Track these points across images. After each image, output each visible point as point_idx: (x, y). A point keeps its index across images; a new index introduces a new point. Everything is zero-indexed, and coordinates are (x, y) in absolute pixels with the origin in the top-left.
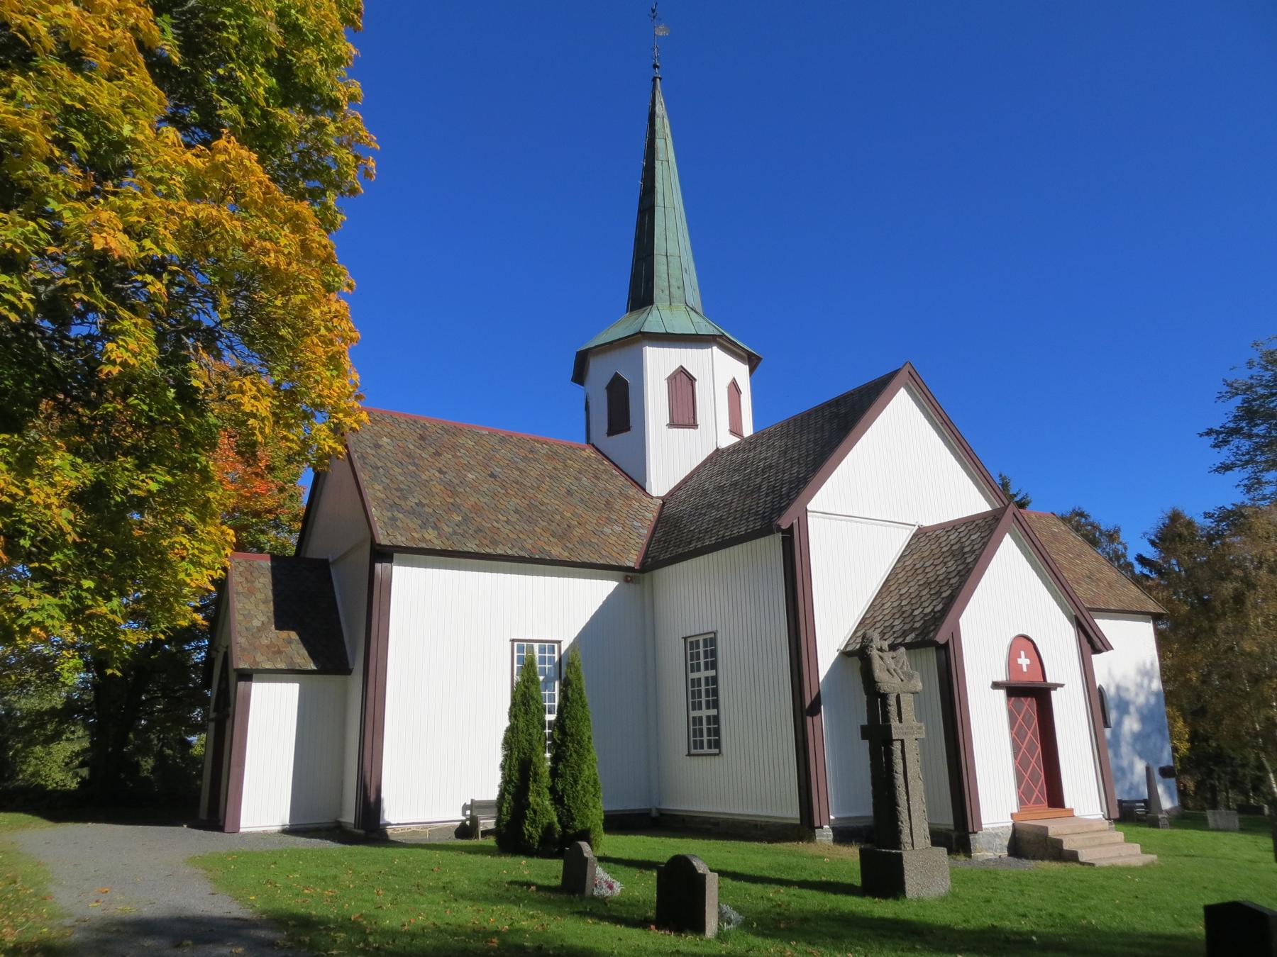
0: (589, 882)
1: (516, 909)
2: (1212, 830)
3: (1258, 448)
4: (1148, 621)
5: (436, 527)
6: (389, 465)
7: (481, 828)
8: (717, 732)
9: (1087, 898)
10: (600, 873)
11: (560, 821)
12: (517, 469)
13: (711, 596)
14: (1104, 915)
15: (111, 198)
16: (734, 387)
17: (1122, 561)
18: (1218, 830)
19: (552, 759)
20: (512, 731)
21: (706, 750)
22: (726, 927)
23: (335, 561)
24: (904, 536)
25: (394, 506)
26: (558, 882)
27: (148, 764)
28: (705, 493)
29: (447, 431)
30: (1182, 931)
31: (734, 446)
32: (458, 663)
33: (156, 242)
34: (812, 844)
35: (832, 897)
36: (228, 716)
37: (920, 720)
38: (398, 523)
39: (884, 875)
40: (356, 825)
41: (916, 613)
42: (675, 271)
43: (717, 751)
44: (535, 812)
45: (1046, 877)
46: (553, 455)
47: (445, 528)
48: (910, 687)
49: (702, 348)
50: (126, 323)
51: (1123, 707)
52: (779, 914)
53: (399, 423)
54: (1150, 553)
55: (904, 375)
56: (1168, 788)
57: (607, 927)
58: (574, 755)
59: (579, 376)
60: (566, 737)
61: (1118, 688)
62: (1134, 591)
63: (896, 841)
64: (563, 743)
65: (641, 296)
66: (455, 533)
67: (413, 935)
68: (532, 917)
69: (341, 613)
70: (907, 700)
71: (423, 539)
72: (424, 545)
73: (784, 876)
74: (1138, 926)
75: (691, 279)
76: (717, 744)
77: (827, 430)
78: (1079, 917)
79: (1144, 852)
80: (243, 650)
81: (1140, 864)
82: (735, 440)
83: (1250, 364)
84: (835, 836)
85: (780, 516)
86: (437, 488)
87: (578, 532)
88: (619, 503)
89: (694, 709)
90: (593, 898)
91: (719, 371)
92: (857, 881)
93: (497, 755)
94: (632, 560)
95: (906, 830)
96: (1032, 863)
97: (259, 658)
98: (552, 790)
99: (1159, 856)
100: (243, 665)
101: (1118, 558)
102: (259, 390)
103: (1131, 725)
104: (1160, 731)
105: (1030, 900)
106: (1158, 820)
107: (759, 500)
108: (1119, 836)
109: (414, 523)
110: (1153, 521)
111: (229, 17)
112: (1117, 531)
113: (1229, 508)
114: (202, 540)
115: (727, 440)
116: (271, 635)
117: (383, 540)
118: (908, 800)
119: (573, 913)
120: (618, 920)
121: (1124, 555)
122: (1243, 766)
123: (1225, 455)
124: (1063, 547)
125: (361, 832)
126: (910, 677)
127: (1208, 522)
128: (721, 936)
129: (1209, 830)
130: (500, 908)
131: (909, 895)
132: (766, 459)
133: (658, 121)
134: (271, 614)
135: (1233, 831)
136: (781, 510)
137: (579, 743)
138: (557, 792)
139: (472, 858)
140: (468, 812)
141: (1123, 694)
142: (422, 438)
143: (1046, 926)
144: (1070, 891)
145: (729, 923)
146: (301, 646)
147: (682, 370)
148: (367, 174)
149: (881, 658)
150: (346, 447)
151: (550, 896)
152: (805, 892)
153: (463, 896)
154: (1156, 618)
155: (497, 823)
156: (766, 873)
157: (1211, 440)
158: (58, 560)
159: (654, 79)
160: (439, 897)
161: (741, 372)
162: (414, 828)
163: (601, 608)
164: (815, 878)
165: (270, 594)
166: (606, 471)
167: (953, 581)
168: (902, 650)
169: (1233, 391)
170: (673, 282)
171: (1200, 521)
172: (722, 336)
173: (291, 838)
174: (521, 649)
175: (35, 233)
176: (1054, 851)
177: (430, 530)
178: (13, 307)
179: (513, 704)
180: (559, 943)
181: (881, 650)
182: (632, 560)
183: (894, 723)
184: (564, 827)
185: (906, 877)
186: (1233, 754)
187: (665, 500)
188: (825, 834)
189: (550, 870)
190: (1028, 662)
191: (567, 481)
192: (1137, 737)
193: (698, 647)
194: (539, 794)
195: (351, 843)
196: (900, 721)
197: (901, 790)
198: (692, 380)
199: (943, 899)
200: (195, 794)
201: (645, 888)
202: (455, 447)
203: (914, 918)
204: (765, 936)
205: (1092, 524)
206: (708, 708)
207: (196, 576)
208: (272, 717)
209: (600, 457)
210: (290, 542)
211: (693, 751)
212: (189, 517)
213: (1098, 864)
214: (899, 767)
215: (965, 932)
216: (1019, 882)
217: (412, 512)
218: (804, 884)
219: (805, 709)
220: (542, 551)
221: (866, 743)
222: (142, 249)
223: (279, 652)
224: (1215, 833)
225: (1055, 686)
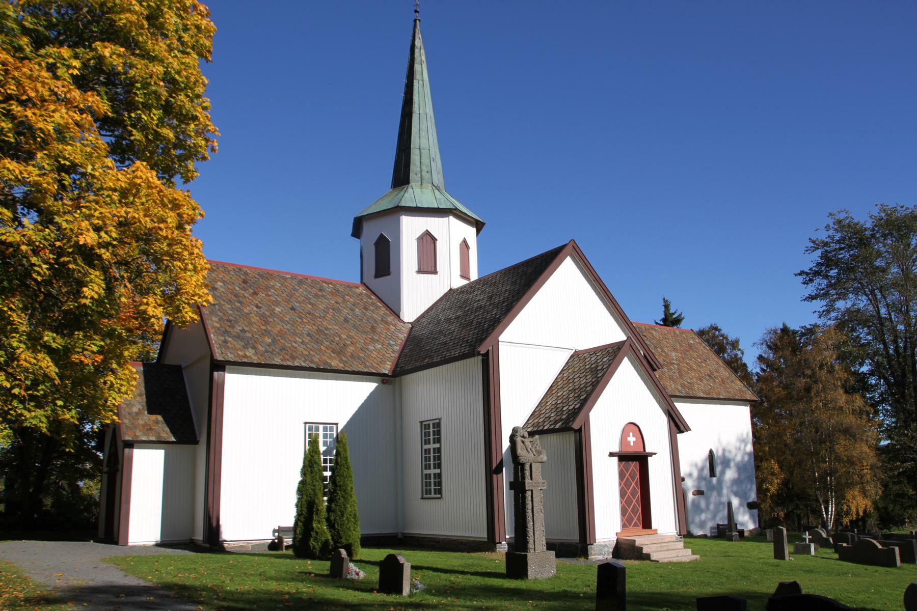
3: (830, 285)
5: (254, 348)
6: (222, 303)
7: (285, 544)
8: (440, 484)
12: (310, 304)
13: (436, 394)
15: (84, 210)
16: (465, 245)
19: (328, 501)
20: (302, 483)
21: (433, 495)
23: (186, 367)
25: (226, 332)
26: (328, 572)
27: (48, 501)
28: (439, 322)
29: (262, 276)
31: (465, 286)
32: (271, 433)
33: (106, 233)
36: (117, 470)
38: (229, 345)
39: (517, 565)
40: (204, 541)
42: (425, 160)
44: (317, 533)
46: (336, 293)
47: (260, 347)
48: (539, 459)
50: (92, 276)
51: (726, 463)
53: (229, 271)
55: (569, 249)
57: (350, 592)
58: (342, 499)
59: (357, 232)
60: (337, 489)
61: (724, 450)
62: (739, 385)
64: (335, 491)
65: (401, 178)
66: (266, 351)
67: (243, 594)
69: (190, 398)
71: (246, 356)
72: (246, 360)
75: (437, 166)
76: (439, 491)
77: (522, 280)
80: (127, 427)
82: (465, 282)
83: (827, 228)
85: (480, 345)
86: (255, 319)
87: (351, 349)
88: (380, 328)
91: (452, 233)
92: (503, 569)
93: (294, 498)
94: (387, 369)
95: (531, 541)
97: (138, 433)
98: (328, 520)
100: (128, 438)
102: (156, 302)
103: (730, 474)
104: (749, 478)
107: (471, 328)
109: (239, 344)
111: (138, 89)
113: (809, 327)
114: (121, 379)
116: (145, 418)
117: (219, 357)
124: (695, 355)
125: (207, 545)
126: (539, 453)
128: (411, 595)
130: (292, 584)
131: (530, 577)
133: (417, 51)
134: (144, 404)
136: (481, 340)
139: (277, 560)
140: (277, 534)
141: (727, 454)
142: (245, 282)
146: (165, 425)
147: (427, 233)
148: (213, 149)
149: (523, 442)
150: (201, 316)
151: (320, 578)
153: (271, 578)
155: (294, 539)
156: (456, 569)
158: (43, 389)
159: (415, 21)
160: (257, 579)
161: (470, 233)
162: (241, 543)
163: (366, 401)
165: (143, 389)
169: (816, 245)
170: (424, 168)
173: (163, 549)
174: (310, 429)
175: (49, 235)
177: (250, 349)
178: (39, 273)
179: (304, 467)
181: (523, 437)
183: (528, 480)
187: (413, 324)
189: (324, 566)
190: (634, 439)
192: (736, 482)
194: (319, 522)
195: (201, 552)
197: (530, 519)
198: (434, 240)
200: (104, 521)
201: (375, 575)
202: (267, 288)
205: (722, 335)
207: (118, 399)
208: (147, 470)
209: (369, 293)
210: (154, 350)
211: (425, 496)
212: (115, 366)
214: (529, 506)
217: (237, 337)
219: (492, 471)
220: (326, 363)
222: (100, 237)
223: (151, 429)
225: (651, 454)
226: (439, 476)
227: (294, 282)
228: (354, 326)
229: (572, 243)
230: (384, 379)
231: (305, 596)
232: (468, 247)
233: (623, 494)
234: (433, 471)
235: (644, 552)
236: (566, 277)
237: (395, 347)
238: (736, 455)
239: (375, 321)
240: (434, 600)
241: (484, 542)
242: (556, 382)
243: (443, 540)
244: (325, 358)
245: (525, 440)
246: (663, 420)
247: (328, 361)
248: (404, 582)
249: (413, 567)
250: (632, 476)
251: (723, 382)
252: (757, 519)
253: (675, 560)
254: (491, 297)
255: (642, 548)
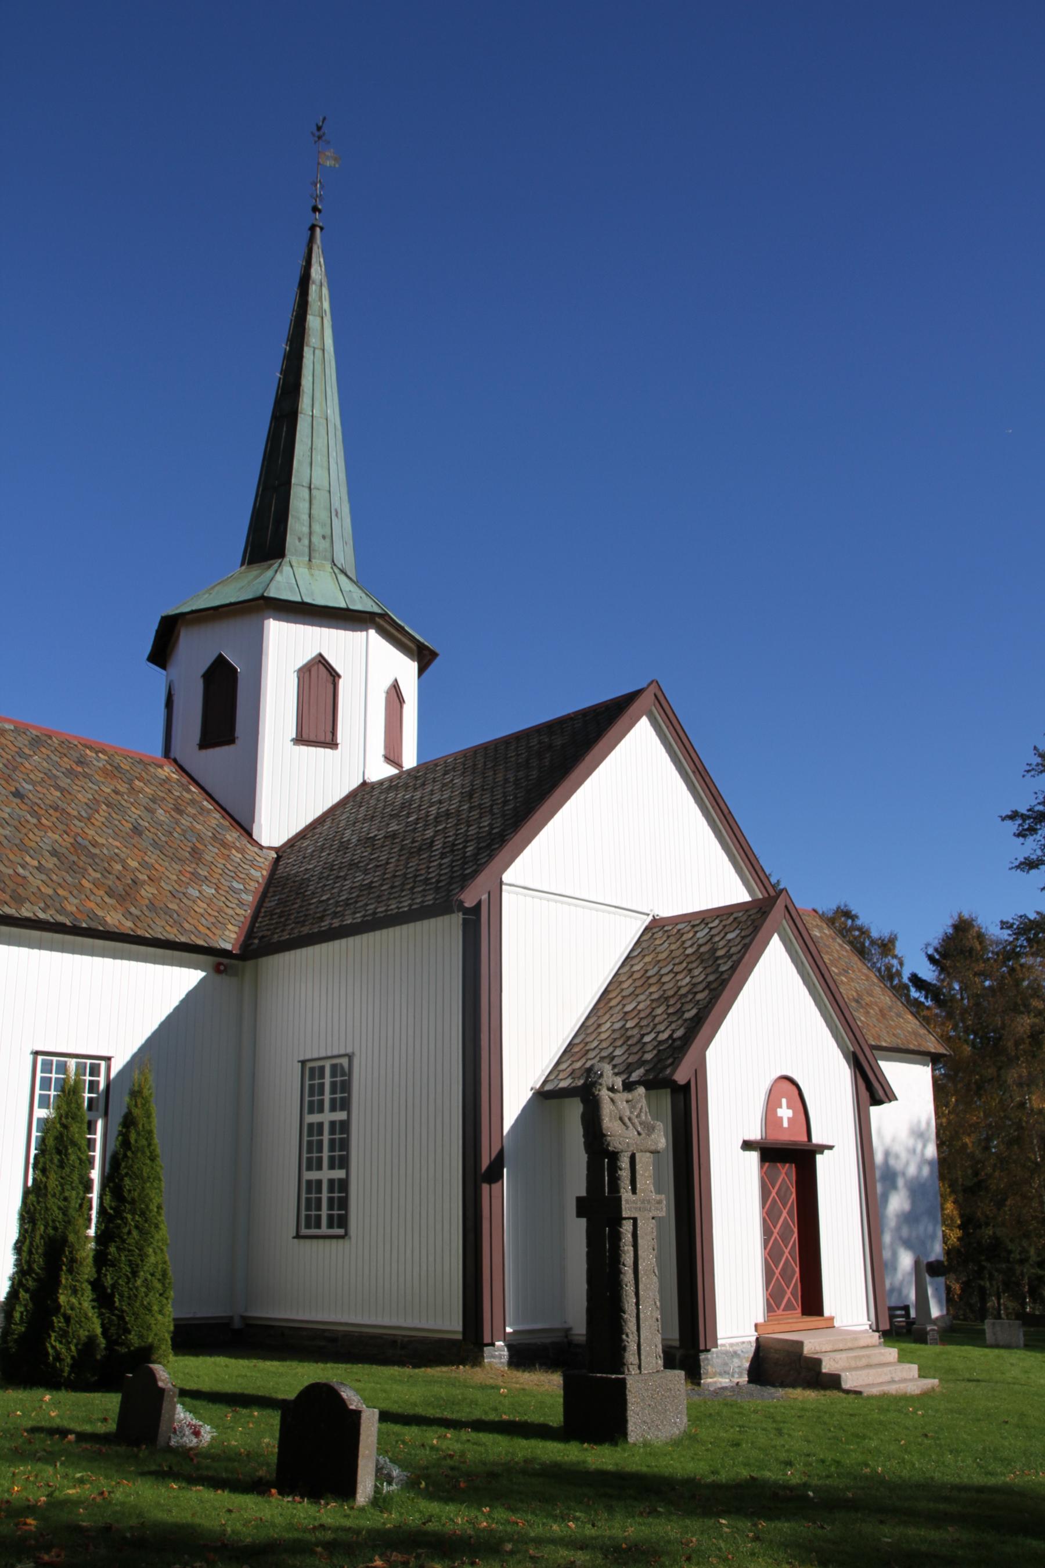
0: (163, 1427)
1: (50, 1469)
2: (991, 1346)
4: (925, 1064)
9: (864, 1437)
10: (182, 1414)
11: (105, 1333)
12: (58, 787)
13: (334, 1002)
14: (893, 1460)
16: (395, 693)
17: (896, 982)
18: (997, 1346)
21: (324, 1230)
22: (386, 1488)
24: (635, 928)
28: (344, 847)
30: (992, 1481)
31: (391, 779)
34: (478, 1369)
35: (524, 1442)
37: (658, 1191)
39: (597, 1407)
41: (647, 1039)
42: (321, 513)
43: (341, 1232)
44: (67, 1319)
45: (803, 1409)
46: (113, 771)
48: (650, 1144)
49: (353, 630)
52: (452, 1468)
54: (928, 973)
55: (646, 700)
56: (936, 1290)
58: (135, 1233)
59: (161, 654)
61: (887, 1154)
62: (911, 1023)
63: (617, 1363)
64: (118, 1213)
65: (267, 542)
68: (81, 1481)
70: (645, 1163)
73: (447, 1414)
74: (937, 1475)
75: (343, 527)
76: (342, 1222)
77: (534, 769)
78: (859, 1464)
79: (921, 1376)
81: (918, 1392)
82: (392, 771)
84: (511, 1356)
85: (463, 888)
87: (148, 891)
88: (211, 852)
89: (309, 1168)
90: (169, 1449)
91: (373, 668)
92: (555, 1417)
94: (229, 939)
95: (632, 1347)
96: (781, 1392)
98: (96, 1285)
99: (941, 1380)
101: (891, 977)
105: (789, 1442)
106: (926, 1333)
108: (891, 1353)
110: (936, 929)
112: (892, 940)
113: (1032, 916)
115: (380, 771)
118: (637, 1304)
119: (143, 1474)
120: (217, 1483)
121: (899, 974)
122: (1022, 1262)
123: (1030, 847)
126: (650, 1129)
127: (1005, 935)
128: (379, 1501)
129: (987, 1347)
131: (631, 1439)
132: (440, 802)
133: (313, 289)
135: (1017, 1347)
136: (465, 880)
137: (143, 1214)
138: (104, 1288)
141: (892, 1162)
143: (820, 1478)
144: (841, 1428)
145: (390, 1483)
147: (321, 661)
151: (95, 1448)
152: (484, 1437)
154: (934, 1059)
156: (420, 1411)
157: (1013, 826)
159: (312, 228)
161: (405, 670)
164: (492, 1417)
166: (193, 802)
167: (699, 997)
168: (641, 1090)
170: (317, 528)
171: (995, 932)
172: (384, 616)
174: (47, 1067)
176: (809, 1373)
180: (133, 1522)
181: (612, 1089)
182: (229, 939)
183: (626, 1194)
184: (111, 1343)
185: (630, 1413)
186: (1010, 1246)
187: (281, 853)
188: (498, 1353)
189: (102, 1409)
191: (135, 812)
193: (322, 1076)
194: (75, 1292)
196: (634, 1191)
197: (629, 1289)
198: (334, 676)
199: (676, 1443)
201: (260, 1435)
203: (644, 1469)
204: (448, 1500)
206: (332, 1167)
209: (185, 780)
211: (304, 1231)
213: (867, 1392)
214: (628, 1258)
215: (716, 1486)
216: (772, 1417)
218: (479, 1426)
219: (480, 1173)
220: (92, 916)
221: (583, 1221)
224: (996, 1351)
225: (822, 1148)
226: (343, 1185)
227: (22, 741)
228: (155, 844)
229: (653, 689)
230: (220, 962)
231: (83, 1518)
232: (401, 700)
233: (767, 1232)
234: (326, 1174)
235: (825, 1370)
236: (639, 755)
237: (244, 896)
238: (907, 1164)
239: (200, 838)
240: (456, 1518)
241: (453, 1342)
242: (616, 981)
243: (347, 1335)
244: (92, 905)
245: (617, 1097)
246: (843, 1073)
247: (100, 913)
248: (361, 1462)
249: (385, 1417)
250: (783, 1197)
251: (883, 1015)
252: (944, 1296)
253: (893, 1389)
254: (471, 795)
255: (818, 1362)
